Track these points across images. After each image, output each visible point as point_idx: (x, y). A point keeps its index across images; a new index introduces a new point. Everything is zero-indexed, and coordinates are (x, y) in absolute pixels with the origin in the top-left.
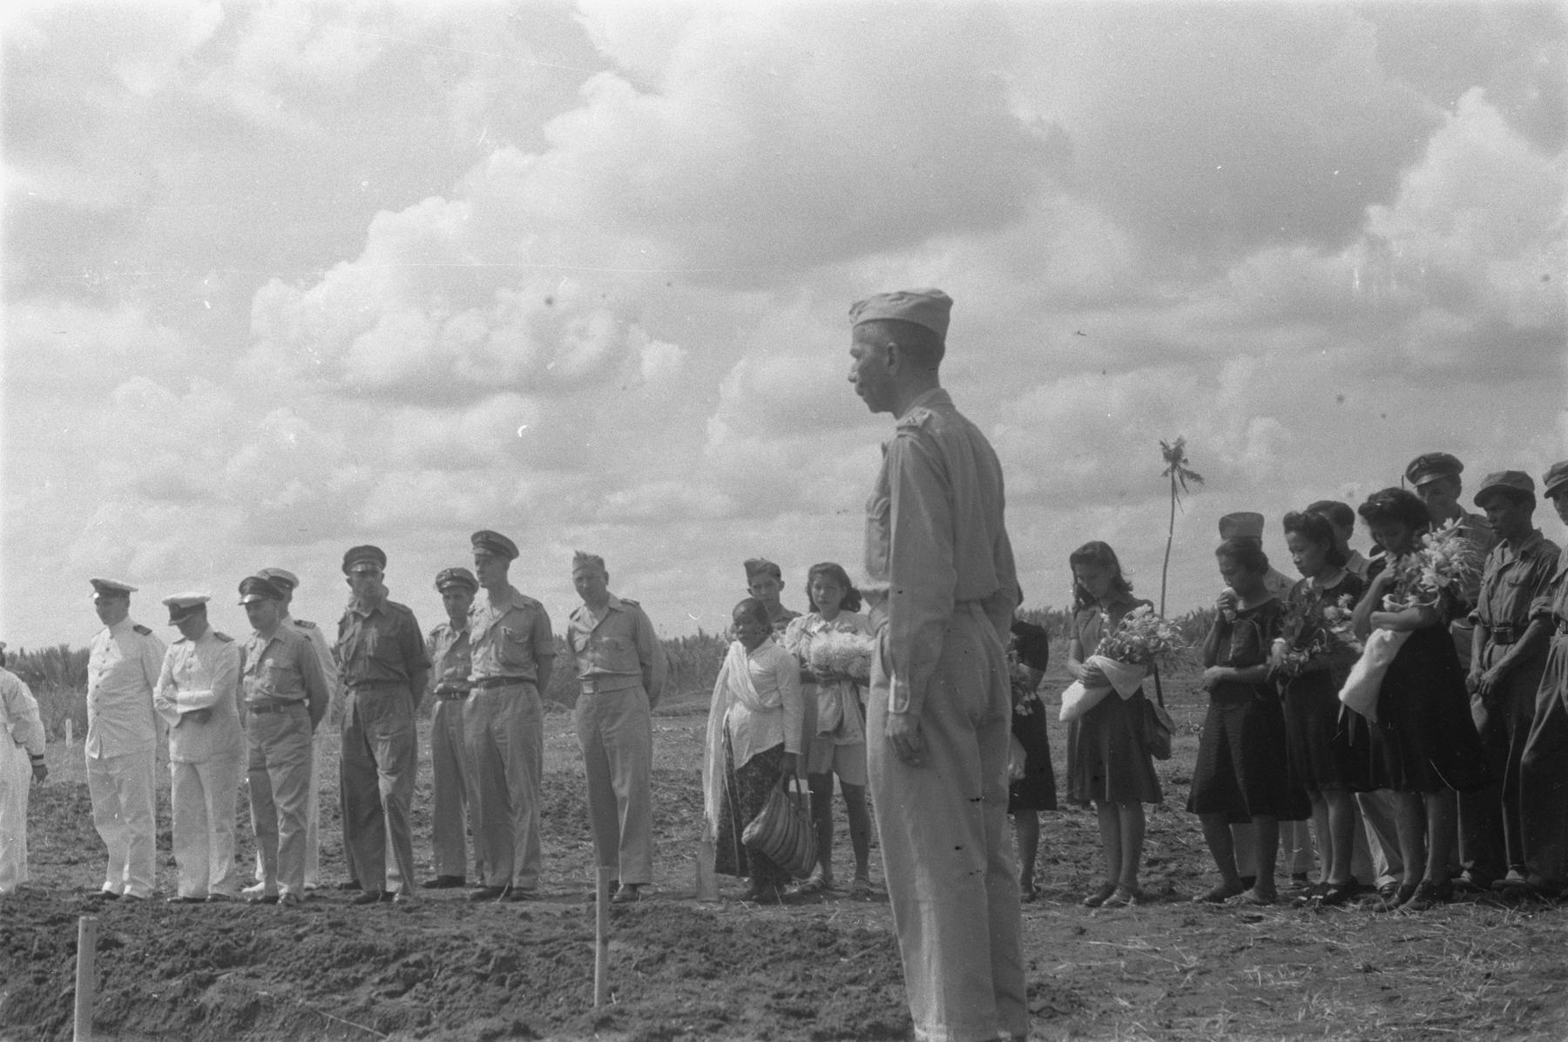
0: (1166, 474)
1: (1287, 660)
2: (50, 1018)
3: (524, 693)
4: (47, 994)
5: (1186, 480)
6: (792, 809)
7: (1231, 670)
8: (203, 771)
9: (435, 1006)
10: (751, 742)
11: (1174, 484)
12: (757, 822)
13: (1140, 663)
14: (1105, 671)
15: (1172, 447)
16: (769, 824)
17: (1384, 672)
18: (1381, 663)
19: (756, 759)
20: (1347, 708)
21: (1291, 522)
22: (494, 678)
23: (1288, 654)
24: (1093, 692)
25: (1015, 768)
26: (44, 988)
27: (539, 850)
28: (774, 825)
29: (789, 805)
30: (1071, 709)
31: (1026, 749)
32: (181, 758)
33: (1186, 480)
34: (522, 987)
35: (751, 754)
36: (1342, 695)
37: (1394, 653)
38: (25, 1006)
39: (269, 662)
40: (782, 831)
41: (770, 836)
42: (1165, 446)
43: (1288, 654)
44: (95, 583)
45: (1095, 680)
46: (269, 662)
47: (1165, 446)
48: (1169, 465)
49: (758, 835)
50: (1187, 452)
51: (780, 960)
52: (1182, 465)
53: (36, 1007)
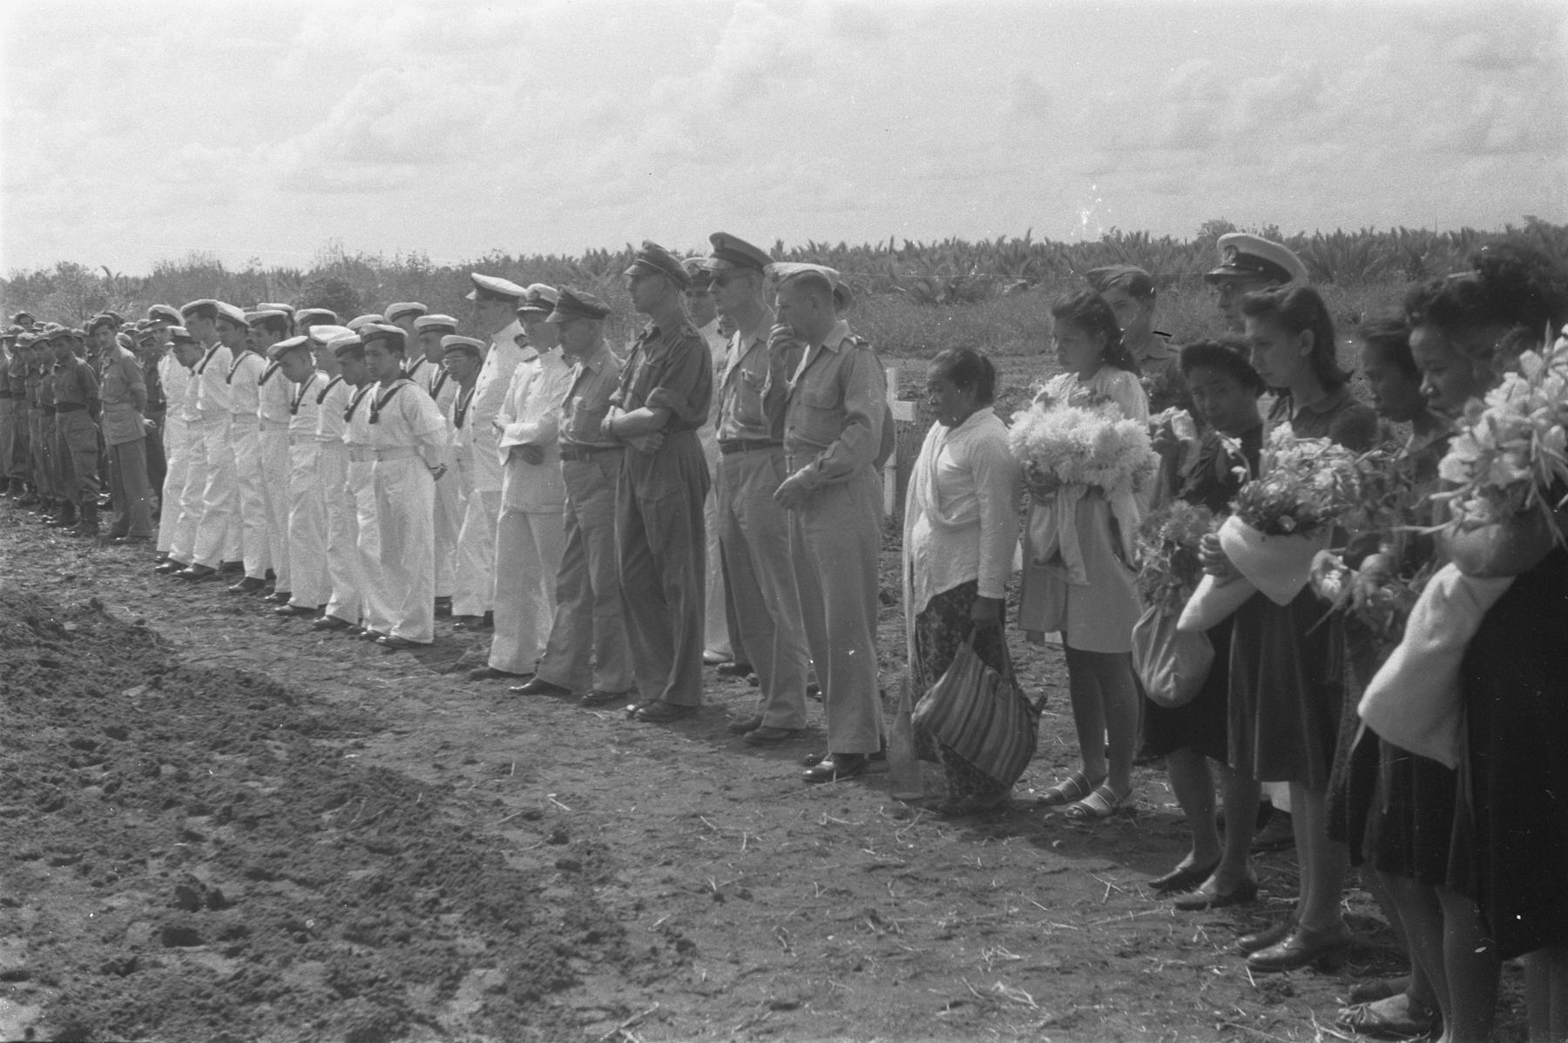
1: (1374, 597)
3: (770, 463)
6: (985, 681)
8: (534, 523)
10: (930, 576)
12: (929, 696)
13: (1294, 532)
14: (1232, 558)
16: (944, 702)
17: (1453, 661)
18: (1434, 643)
19: (936, 600)
20: (1368, 731)
21: (1152, 412)
22: (731, 440)
23: (1380, 584)
25: (1166, 679)
28: (952, 703)
29: (982, 670)
31: (1216, 648)
35: (930, 596)
36: (1362, 707)
37: (1470, 626)
39: (577, 399)
40: (961, 713)
41: (944, 718)
43: (1380, 584)
44: (629, 246)
46: (577, 399)
49: (924, 716)
51: (985, 904)
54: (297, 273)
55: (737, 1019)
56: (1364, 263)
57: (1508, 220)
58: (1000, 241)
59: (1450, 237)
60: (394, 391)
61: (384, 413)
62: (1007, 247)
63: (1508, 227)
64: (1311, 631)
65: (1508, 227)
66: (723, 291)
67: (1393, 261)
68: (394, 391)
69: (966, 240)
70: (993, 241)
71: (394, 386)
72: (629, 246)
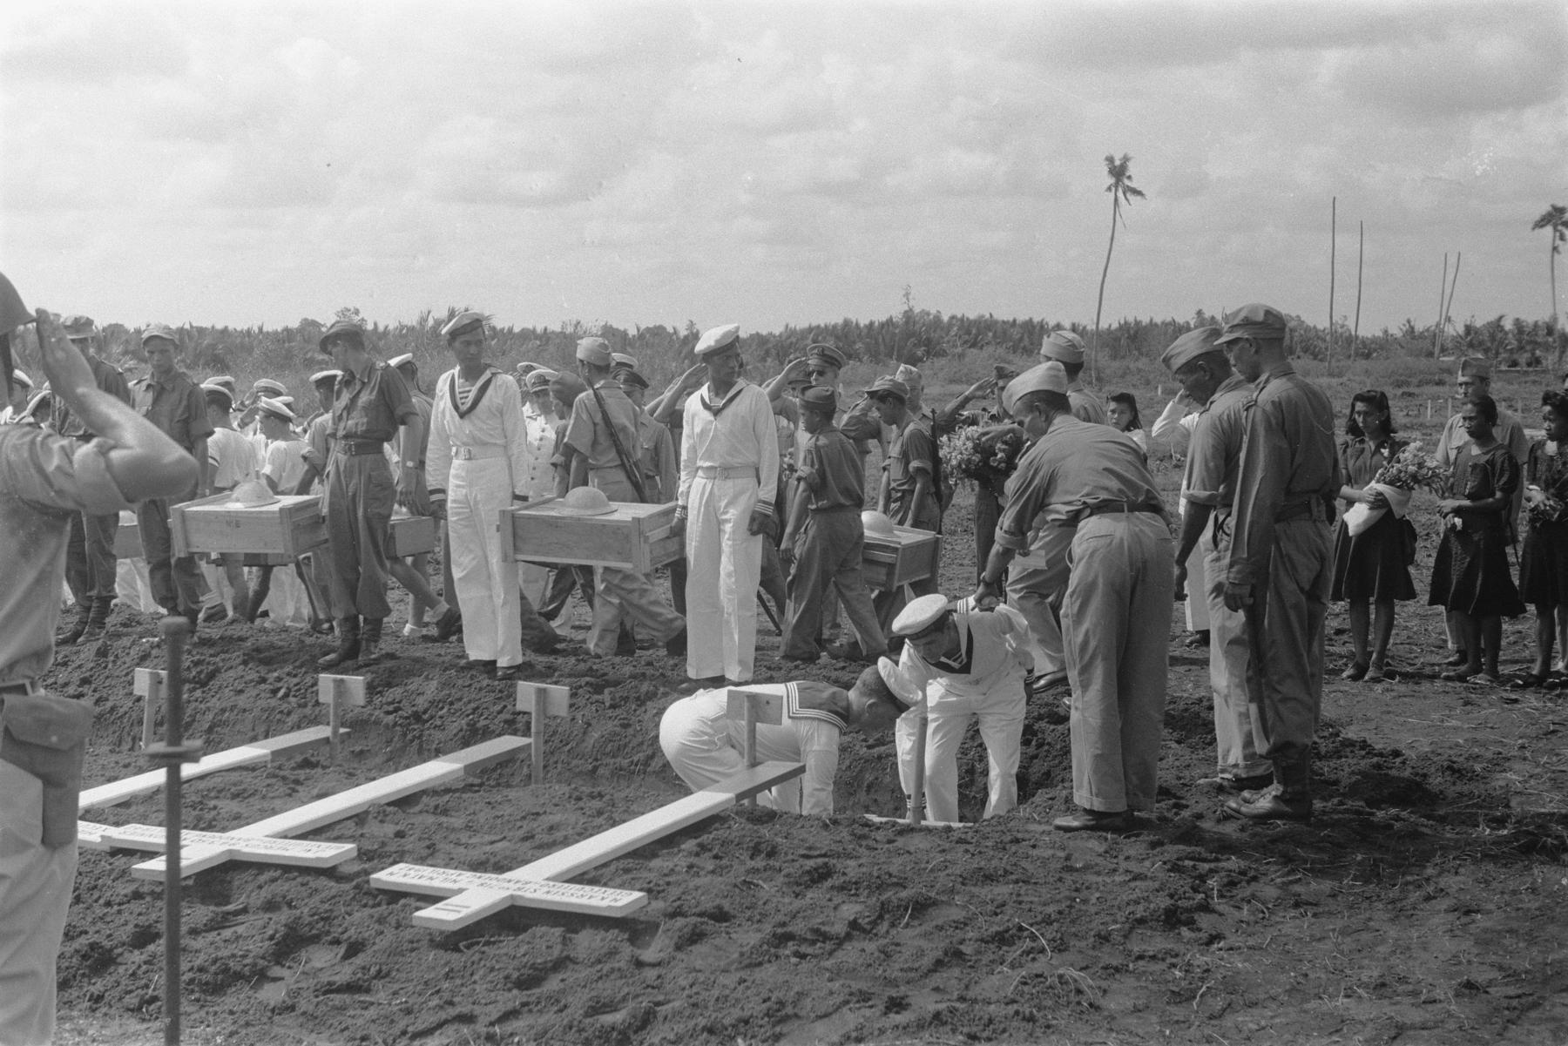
0: (1109, 189)
2: (641, 755)
4: (634, 736)
5: (1128, 195)
7: (1467, 503)
9: (977, 758)
11: (1116, 200)
15: (1117, 163)
24: (1375, 513)
26: (630, 731)
27: (863, 533)
30: (1358, 526)
32: (1098, 805)
33: (1128, 195)
34: (1046, 748)
38: (616, 744)
42: (1110, 160)
45: (1379, 502)
47: (1110, 160)
48: (1112, 181)
50: (1132, 169)
52: (1126, 182)
53: (625, 746)
66: (821, 379)
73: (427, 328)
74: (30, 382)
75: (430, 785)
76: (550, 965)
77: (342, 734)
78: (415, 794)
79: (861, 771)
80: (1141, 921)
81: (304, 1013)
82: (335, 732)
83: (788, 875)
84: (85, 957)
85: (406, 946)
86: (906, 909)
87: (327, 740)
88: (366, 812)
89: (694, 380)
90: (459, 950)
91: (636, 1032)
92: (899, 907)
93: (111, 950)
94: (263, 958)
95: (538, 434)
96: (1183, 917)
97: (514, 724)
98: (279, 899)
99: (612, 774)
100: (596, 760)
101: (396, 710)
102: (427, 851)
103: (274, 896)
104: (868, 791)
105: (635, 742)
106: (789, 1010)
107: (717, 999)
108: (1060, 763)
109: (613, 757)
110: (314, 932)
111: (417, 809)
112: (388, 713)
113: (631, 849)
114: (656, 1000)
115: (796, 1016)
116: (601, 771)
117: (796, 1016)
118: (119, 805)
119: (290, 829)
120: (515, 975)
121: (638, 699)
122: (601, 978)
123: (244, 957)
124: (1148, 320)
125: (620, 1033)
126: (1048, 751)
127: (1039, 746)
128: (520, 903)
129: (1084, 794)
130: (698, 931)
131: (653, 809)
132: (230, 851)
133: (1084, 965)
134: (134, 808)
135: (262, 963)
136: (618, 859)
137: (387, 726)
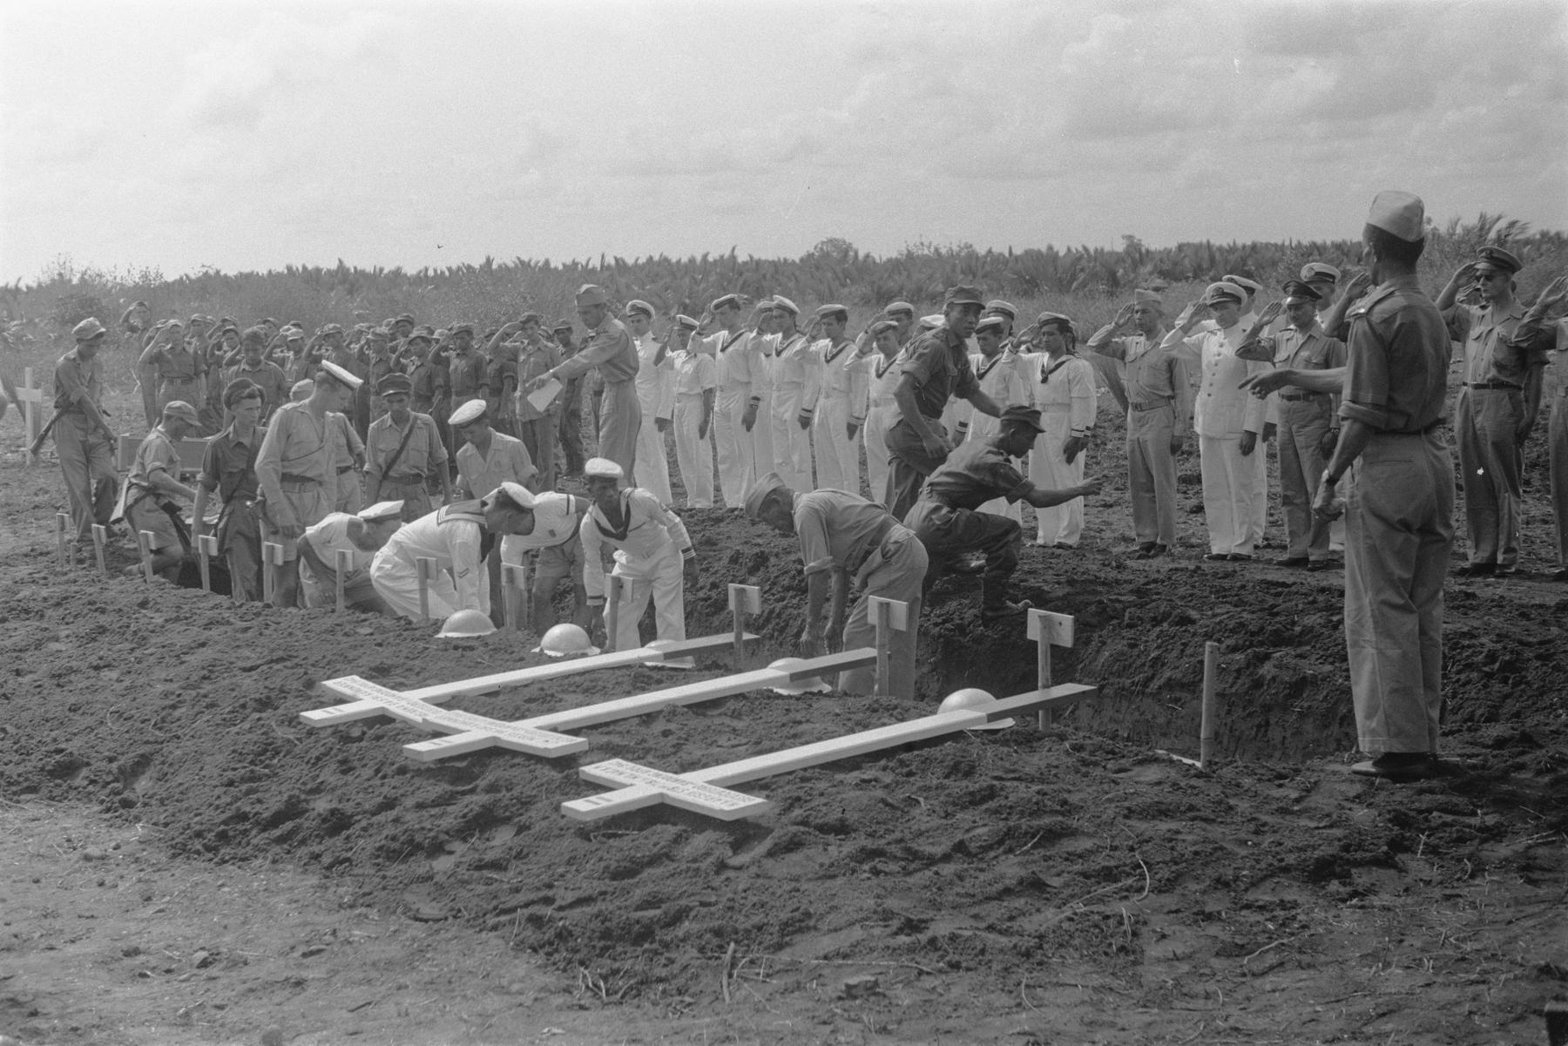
26: (1136, 652)
44: (340, 261)
53: (1130, 666)
54: (469, 267)
55: (403, 703)
56: (1073, 278)
57: (289, 262)
58: (705, 256)
59: (447, 273)
60: (1063, 363)
61: (1052, 377)
62: (1017, 258)
63: (1050, 248)
64: (315, 528)
65: (1050, 248)
66: (1489, 284)
67: (1094, 276)
68: (1063, 363)
69: (1035, 247)
70: (699, 258)
71: (1063, 358)
72: (340, 261)
73: (1456, 237)
74: (797, 309)
75: (744, 690)
76: (646, 860)
77: (748, 642)
78: (726, 697)
79: (1335, 703)
80: (1286, 870)
81: (436, 883)
82: (739, 637)
83: (949, 795)
84: (324, 820)
85: (556, 832)
86: (1033, 836)
87: (730, 645)
88: (661, 712)
89: (1357, 290)
90: (590, 840)
91: (662, 928)
92: (1026, 833)
93: (352, 816)
94: (447, 833)
95: (1215, 349)
96: (1338, 870)
97: (865, 635)
98: (501, 783)
99: (1116, 694)
100: (1104, 679)
101: (944, 622)
102: (673, 750)
103: (496, 780)
104: (1341, 724)
105: (1138, 663)
106: (812, 923)
107: (754, 905)
108: (1534, 704)
109: (1119, 676)
110: (507, 814)
111: (719, 711)
112: (936, 625)
113: (830, 759)
114: (705, 899)
115: (815, 928)
116: (1106, 691)
117: (815, 928)
118: (486, 695)
119: (560, 724)
120: (614, 865)
121: (1154, 619)
122: (673, 875)
123: (430, 830)
124: (265, 272)
125: (643, 927)
126: (1523, 691)
127: (1515, 685)
128: (667, 802)
129: (1370, 736)
130: (796, 840)
131: (476, 712)
132: (494, 738)
133: (1174, 908)
134: (501, 697)
135: (443, 837)
136: (813, 767)
137: (933, 637)
